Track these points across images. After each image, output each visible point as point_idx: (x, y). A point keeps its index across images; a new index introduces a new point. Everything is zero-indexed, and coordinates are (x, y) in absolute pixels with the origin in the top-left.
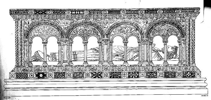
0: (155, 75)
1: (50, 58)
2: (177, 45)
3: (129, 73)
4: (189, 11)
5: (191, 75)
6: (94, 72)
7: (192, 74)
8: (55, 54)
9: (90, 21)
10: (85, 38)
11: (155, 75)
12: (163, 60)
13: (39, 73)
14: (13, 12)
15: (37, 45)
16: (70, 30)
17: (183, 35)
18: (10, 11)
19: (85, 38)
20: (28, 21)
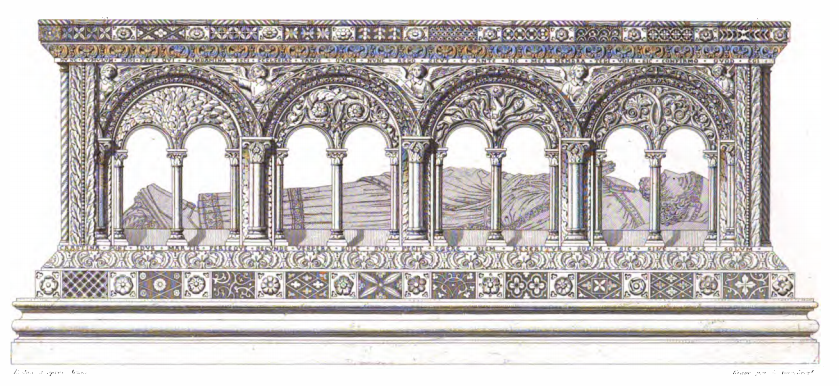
0: (615, 286)
1: (195, 214)
2: (702, 167)
3: (509, 277)
4: (741, 34)
5: (754, 288)
6: (370, 274)
7: (758, 284)
8: (215, 197)
9: (324, 70)
10: (336, 126)
11: (613, 289)
12: (646, 227)
13: (152, 276)
14: (67, 39)
15: (144, 160)
16: (597, 105)
17: (726, 125)
18: (41, 24)
19: (336, 126)
20: (114, 76)
